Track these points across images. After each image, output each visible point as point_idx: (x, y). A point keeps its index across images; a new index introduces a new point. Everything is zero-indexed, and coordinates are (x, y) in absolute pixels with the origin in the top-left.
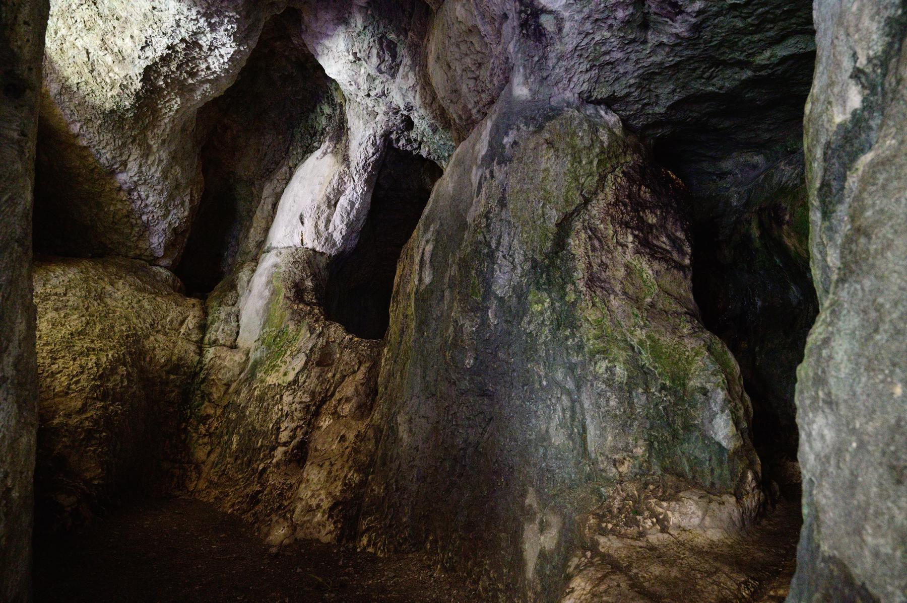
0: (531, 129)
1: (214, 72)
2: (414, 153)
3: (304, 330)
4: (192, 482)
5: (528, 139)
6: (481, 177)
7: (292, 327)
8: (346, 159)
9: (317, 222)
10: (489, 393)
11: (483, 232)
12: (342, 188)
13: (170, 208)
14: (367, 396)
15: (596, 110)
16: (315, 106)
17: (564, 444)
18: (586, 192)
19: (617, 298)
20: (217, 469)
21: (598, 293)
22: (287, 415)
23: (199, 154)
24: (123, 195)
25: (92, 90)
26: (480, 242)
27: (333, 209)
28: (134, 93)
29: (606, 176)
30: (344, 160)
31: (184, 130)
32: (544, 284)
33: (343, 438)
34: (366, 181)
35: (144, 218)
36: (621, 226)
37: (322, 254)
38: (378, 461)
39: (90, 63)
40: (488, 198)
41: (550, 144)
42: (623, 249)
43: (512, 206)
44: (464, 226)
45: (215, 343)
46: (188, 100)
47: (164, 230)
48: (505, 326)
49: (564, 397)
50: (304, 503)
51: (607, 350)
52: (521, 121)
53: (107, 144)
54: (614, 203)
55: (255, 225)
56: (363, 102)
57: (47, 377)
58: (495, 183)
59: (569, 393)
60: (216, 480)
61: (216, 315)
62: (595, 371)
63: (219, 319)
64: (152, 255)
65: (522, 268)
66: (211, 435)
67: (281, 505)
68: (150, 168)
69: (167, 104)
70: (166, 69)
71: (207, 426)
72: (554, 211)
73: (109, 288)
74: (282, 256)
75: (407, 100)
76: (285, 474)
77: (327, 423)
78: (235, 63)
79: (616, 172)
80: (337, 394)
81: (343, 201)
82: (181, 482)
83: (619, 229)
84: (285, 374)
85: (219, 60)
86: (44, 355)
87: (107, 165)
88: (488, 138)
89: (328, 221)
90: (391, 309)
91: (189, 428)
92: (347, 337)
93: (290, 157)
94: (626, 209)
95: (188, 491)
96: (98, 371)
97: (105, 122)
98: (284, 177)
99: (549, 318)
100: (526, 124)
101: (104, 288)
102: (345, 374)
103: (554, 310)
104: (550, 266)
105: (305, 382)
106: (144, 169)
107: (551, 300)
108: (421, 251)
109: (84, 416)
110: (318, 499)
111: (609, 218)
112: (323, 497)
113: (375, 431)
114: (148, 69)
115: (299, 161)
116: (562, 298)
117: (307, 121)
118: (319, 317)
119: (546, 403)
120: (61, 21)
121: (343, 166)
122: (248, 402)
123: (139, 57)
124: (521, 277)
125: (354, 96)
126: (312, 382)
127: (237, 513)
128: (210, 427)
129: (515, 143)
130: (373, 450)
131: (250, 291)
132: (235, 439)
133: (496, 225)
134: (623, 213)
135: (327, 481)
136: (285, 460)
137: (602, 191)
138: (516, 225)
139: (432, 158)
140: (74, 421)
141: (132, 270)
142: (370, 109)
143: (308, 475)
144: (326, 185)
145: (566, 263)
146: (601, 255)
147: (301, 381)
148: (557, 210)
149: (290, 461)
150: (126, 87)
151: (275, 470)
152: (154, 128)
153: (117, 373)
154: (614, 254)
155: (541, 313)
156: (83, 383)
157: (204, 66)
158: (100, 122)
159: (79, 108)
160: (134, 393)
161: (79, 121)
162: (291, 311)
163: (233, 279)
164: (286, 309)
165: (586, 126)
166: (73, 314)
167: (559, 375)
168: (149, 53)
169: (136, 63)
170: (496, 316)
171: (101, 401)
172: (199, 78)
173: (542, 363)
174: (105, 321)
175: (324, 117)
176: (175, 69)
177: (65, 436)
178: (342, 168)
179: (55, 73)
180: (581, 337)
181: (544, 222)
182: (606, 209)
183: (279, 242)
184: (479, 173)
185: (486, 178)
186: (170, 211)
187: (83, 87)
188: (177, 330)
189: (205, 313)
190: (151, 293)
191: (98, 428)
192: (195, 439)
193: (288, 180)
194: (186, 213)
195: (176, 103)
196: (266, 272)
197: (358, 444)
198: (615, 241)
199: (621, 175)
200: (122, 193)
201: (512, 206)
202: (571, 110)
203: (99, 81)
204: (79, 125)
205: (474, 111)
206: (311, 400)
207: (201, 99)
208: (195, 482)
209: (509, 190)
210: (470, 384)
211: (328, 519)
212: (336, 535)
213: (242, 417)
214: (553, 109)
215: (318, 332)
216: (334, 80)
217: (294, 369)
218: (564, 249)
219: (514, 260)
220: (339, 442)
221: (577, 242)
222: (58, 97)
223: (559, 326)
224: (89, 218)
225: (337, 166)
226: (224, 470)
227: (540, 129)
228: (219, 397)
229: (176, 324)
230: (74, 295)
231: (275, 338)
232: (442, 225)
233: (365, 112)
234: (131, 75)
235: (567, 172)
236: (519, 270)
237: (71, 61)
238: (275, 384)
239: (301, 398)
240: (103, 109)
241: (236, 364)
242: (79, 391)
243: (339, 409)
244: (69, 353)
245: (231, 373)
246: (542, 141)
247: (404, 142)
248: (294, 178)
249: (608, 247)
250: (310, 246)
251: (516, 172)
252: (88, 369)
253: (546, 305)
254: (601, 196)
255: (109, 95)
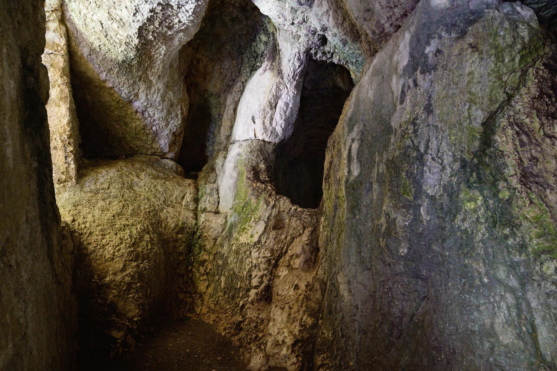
0: (453, 35)
1: (184, 24)
2: (328, 61)
3: (262, 202)
4: (198, 307)
5: (452, 45)
6: (404, 86)
7: (253, 200)
8: (280, 72)
9: (264, 121)
10: (423, 277)
11: (411, 137)
12: (279, 94)
13: (169, 120)
14: (312, 253)
15: (512, 6)
16: (255, 37)
17: (513, 343)
18: (509, 89)
19: (553, 192)
20: (213, 299)
21: (533, 189)
22: (255, 266)
23: (183, 81)
24: (139, 115)
25: (109, 49)
26: (409, 147)
27: (274, 110)
28: (135, 47)
29: (527, 71)
30: (279, 73)
31: (171, 66)
32: (475, 182)
33: (297, 287)
34: (296, 87)
35: (154, 128)
36: (547, 118)
37: (269, 143)
38: (325, 309)
39: (104, 30)
40: (414, 105)
41: (474, 47)
42: (551, 140)
43: (438, 112)
44: (389, 130)
45: (204, 210)
46: (170, 46)
47: (167, 135)
48: (437, 221)
49: (508, 295)
50: (273, 338)
51: (553, 250)
52: (442, 29)
53: (124, 84)
54: (539, 96)
55: (223, 124)
56: (289, 29)
57: (100, 248)
58: (421, 91)
59: (512, 290)
60: (213, 308)
61: (204, 191)
62: (542, 272)
63: (206, 193)
64: (162, 152)
65: (452, 168)
66: (207, 274)
67: (257, 336)
68: (153, 96)
69: (157, 51)
70: (152, 27)
71: (205, 268)
72: (480, 111)
73: (136, 179)
74: (243, 148)
75: (323, 23)
76: (258, 309)
77: (284, 273)
78: (197, 15)
79: (537, 65)
80: (289, 252)
81: (281, 104)
82: (191, 307)
83: (546, 121)
84: (252, 236)
85: (186, 15)
86: (97, 233)
87: (126, 97)
88: (408, 49)
89: (272, 119)
90: (323, 187)
91: (194, 269)
92: (293, 208)
93: (242, 75)
94: (550, 100)
95: (196, 314)
96: (131, 241)
97: (120, 70)
98: (239, 90)
99: (484, 216)
100: (447, 31)
101: (133, 180)
102: (294, 236)
103: (487, 208)
104: (479, 164)
105: (266, 242)
106: (149, 97)
107: (484, 197)
108: (348, 148)
109: (124, 274)
110: (283, 336)
111: (534, 112)
112: (286, 334)
113: (320, 284)
114: (140, 29)
115: (248, 78)
116: (495, 195)
117: (251, 48)
118: (272, 193)
119: (489, 300)
120: (81, 4)
121: (279, 78)
122: (229, 254)
123: (134, 22)
124: (450, 177)
125: (282, 26)
126: (271, 243)
127: (228, 336)
128: (206, 269)
129: (438, 51)
130: (320, 299)
131: (224, 172)
132: (223, 279)
133: (423, 130)
134: (548, 105)
135: (288, 322)
136: (257, 299)
137: (524, 86)
138: (444, 129)
139: (342, 64)
140: (119, 278)
141: (151, 164)
142: (294, 34)
143: (274, 315)
144: (268, 92)
145: (495, 160)
146: (531, 149)
147: (263, 242)
148: (482, 110)
149: (261, 299)
150: (129, 44)
151: (251, 306)
152: (152, 68)
153: (144, 240)
154: (542, 147)
155: (475, 211)
156: (123, 250)
157: (176, 21)
158: (117, 70)
159: (103, 63)
160: (156, 252)
161: (105, 71)
162: (252, 188)
163: (213, 164)
164: (248, 187)
165: (507, 25)
166: (114, 201)
167: (501, 273)
168: (139, 17)
169: (132, 25)
170: (428, 213)
171: (135, 261)
172: (175, 30)
173: (481, 261)
174: (135, 203)
175: (262, 43)
176: (158, 26)
177: (114, 289)
178: (278, 79)
179: (84, 41)
180: (522, 237)
181: (470, 123)
182: (531, 103)
183: (240, 137)
184: (402, 82)
185: (409, 87)
186: (169, 122)
187: (103, 48)
188: (180, 203)
189: (197, 190)
190: (163, 179)
191: (134, 280)
192: (198, 276)
193: (242, 92)
194: (180, 122)
195: (163, 49)
196: (233, 159)
197: (308, 292)
198: (542, 133)
199: (542, 68)
200: (138, 114)
201: (438, 112)
202: (491, 11)
203: (112, 42)
204: (105, 73)
205: (387, 25)
206: (271, 256)
207: (179, 44)
208: (200, 308)
209: (435, 97)
210: (404, 268)
211: (291, 354)
212: (299, 366)
213: (226, 264)
214: (473, 13)
215: (272, 204)
216: (267, 16)
217: (257, 233)
218: (490, 146)
219: (443, 161)
220: (294, 289)
221: (504, 139)
222: (89, 57)
223: (495, 223)
224: (121, 132)
225: (274, 79)
226: (218, 301)
227: (463, 34)
228: (210, 248)
229: (179, 199)
230: (114, 188)
231: (243, 208)
232: (365, 126)
233: (291, 36)
234: (131, 35)
235: (491, 72)
236: (448, 170)
237: (92, 31)
238: (245, 243)
239: (264, 254)
240: (117, 61)
241: (219, 226)
242: (121, 256)
243: (292, 262)
244: (113, 230)
245: (216, 231)
246: (466, 46)
247: (321, 54)
248: (246, 90)
249: (536, 140)
250: (261, 138)
251: (441, 79)
252: (125, 240)
253: (479, 203)
254: (523, 90)
255: (120, 51)
